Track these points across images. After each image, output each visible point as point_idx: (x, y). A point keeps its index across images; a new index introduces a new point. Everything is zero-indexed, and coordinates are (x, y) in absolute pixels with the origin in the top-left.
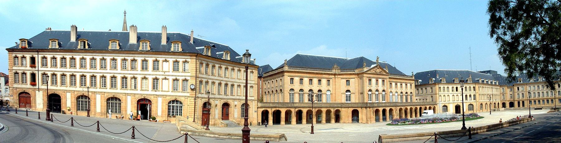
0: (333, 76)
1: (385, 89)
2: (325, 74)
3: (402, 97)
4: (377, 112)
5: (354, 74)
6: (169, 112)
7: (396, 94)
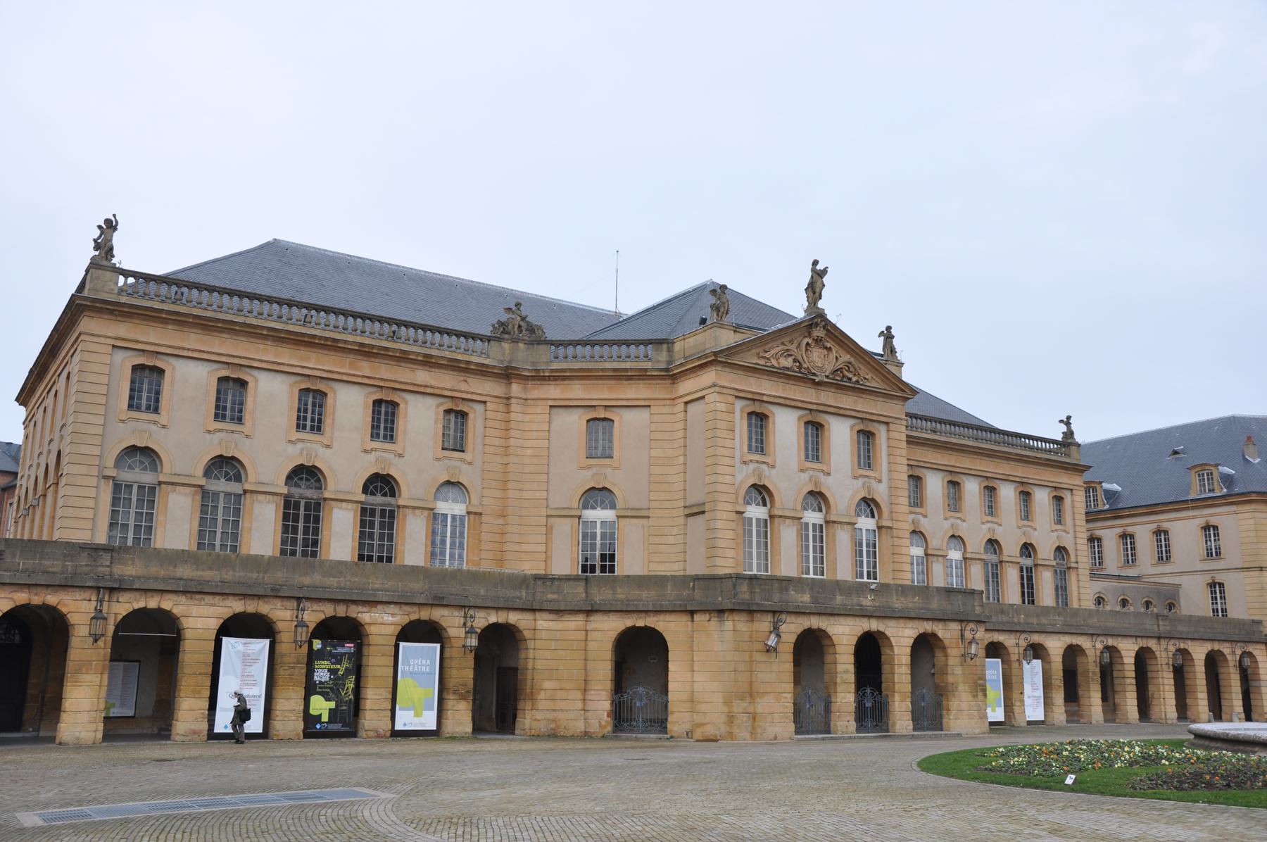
1: (881, 492)
2: (428, 362)
3: (994, 574)
4: (811, 648)
7: (955, 555)
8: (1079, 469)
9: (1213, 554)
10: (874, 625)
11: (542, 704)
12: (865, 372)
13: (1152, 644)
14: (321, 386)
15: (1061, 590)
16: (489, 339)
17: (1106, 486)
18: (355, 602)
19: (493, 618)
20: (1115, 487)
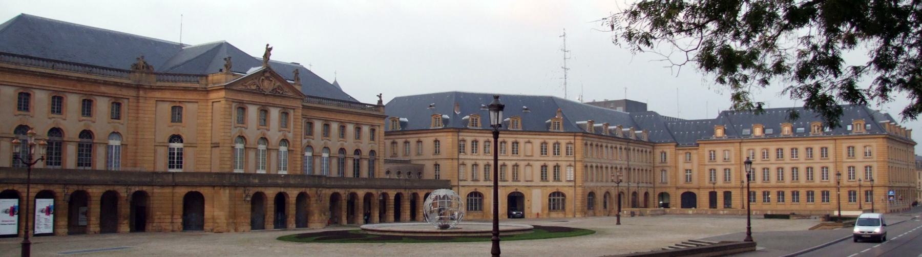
0: (132, 93)
1: (290, 136)
2: (106, 83)
3: (342, 163)
4: (258, 199)
5: (195, 90)
6: (550, 204)
7: (325, 155)
8: (383, 117)
9: (437, 152)
10: (282, 190)
11: (156, 221)
12: (286, 89)
13: (402, 191)
14: (61, 95)
15: (371, 168)
16: (129, 72)
17: (401, 119)
18: (86, 185)
19: (137, 189)
20: (406, 120)
